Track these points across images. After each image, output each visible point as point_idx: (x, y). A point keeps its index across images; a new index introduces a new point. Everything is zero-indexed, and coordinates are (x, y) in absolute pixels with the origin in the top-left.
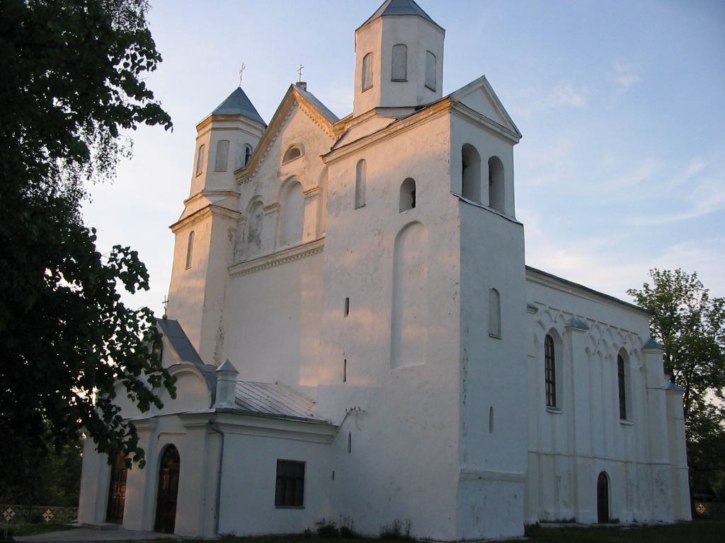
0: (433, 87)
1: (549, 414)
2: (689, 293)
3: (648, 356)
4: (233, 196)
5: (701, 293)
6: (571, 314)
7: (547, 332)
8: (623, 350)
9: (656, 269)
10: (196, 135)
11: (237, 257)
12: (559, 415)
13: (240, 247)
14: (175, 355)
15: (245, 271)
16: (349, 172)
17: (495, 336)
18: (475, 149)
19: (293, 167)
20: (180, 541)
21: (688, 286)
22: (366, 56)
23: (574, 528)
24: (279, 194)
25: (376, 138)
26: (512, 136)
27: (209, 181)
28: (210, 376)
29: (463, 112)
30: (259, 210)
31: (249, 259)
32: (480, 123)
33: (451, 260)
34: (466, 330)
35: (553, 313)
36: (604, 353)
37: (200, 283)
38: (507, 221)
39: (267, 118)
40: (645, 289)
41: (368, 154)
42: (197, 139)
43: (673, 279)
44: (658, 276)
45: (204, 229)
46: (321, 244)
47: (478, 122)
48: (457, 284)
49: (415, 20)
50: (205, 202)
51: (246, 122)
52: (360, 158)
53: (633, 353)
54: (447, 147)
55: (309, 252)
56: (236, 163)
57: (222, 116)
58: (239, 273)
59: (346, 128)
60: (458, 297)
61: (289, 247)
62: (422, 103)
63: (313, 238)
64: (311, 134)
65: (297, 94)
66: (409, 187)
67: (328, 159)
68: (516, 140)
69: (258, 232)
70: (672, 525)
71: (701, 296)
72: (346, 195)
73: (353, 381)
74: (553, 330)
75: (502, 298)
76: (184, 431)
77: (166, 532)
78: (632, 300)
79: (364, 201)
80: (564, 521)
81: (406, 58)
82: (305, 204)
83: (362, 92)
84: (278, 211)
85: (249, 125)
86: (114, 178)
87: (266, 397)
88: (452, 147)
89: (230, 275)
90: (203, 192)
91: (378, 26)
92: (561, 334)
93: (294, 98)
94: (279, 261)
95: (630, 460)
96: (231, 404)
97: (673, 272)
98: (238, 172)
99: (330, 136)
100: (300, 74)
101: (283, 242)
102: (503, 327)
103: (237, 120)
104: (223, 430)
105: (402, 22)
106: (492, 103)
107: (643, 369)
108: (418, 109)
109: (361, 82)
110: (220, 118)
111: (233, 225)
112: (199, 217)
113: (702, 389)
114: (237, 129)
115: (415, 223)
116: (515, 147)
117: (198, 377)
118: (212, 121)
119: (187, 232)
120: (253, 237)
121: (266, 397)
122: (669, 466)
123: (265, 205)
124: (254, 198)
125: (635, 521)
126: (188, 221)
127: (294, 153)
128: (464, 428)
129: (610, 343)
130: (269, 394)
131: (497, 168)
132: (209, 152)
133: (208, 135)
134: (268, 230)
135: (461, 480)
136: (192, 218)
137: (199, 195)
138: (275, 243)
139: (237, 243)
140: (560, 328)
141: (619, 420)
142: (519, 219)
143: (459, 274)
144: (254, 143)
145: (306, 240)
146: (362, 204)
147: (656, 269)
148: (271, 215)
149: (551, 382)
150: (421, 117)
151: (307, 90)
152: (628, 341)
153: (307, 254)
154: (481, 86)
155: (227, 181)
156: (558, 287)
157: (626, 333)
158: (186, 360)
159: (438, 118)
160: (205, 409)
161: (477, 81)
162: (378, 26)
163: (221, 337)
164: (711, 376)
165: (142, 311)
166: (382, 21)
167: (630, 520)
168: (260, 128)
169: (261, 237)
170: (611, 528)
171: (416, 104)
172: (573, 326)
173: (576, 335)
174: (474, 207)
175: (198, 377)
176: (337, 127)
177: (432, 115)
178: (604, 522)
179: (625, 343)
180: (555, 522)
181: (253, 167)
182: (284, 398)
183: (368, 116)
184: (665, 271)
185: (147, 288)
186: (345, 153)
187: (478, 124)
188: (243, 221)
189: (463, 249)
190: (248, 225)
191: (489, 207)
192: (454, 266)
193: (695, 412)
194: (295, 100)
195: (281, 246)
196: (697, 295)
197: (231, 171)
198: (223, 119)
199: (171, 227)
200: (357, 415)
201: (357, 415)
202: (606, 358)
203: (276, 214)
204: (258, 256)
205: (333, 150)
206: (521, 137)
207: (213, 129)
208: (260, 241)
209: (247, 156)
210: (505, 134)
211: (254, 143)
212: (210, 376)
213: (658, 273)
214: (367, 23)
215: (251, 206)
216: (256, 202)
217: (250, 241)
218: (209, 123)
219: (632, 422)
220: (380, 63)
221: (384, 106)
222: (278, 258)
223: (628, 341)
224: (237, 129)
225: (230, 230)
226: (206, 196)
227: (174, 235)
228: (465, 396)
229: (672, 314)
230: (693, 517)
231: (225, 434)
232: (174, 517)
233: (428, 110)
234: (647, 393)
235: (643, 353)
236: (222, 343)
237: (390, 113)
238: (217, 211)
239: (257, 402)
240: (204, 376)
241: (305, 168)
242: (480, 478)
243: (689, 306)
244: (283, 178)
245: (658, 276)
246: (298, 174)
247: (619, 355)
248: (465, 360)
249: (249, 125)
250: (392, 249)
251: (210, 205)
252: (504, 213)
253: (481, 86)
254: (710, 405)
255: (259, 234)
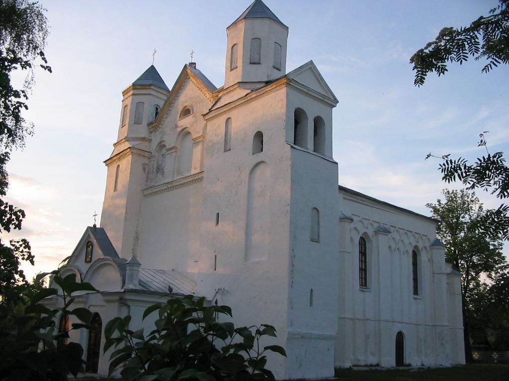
0: (279, 67)
1: (362, 292)
2: (470, 206)
3: (434, 251)
4: (147, 141)
5: (478, 206)
6: (378, 223)
7: (361, 235)
8: (416, 247)
9: (447, 189)
10: (122, 98)
11: (148, 183)
12: (368, 293)
13: (150, 176)
14: (100, 252)
15: (154, 193)
16: (221, 126)
17: (315, 240)
18: (302, 110)
19: (186, 122)
20: (98, 378)
21: (469, 201)
22: (234, 46)
23: (377, 371)
24: (177, 139)
25: (238, 103)
26: (331, 101)
27: (129, 131)
28: (122, 266)
29: (296, 86)
30: (164, 151)
31: (156, 185)
32: (308, 94)
33: (284, 190)
34: (294, 237)
35: (366, 222)
36: (402, 250)
37: (122, 202)
38: (326, 161)
39: (170, 84)
40: (438, 203)
41: (233, 114)
42: (123, 101)
43: (459, 196)
44: (448, 194)
45: (126, 163)
46: (202, 175)
47: (306, 92)
48: (288, 205)
49: (267, 21)
50: (127, 145)
51: (155, 89)
52: (228, 117)
53: (424, 249)
54: (284, 110)
55: (195, 180)
56: (148, 119)
57: (139, 85)
58: (150, 194)
59: (220, 96)
60: (288, 214)
61: (182, 177)
62: (271, 79)
63: (198, 171)
64: (198, 99)
65: (189, 71)
66: (259, 136)
67: (207, 117)
68: (334, 105)
69: (163, 165)
70: (447, 368)
71: (478, 208)
72: (218, 142)
73: (220, 270)
74: (365, 233)
75: (321, 214)
76: (105, 304)
77: (92, 372)
78: (429, 213)
79: (230, 147)
80: (371, 365)
81: (260, 48)
82: (193, 147)
83: (230, 71)
84: (176, 151)
85: (157, 91)
86: (24, 147)
87: (163, 280)
88: (287, 110)
89: (144, 195)
90: (126, 138)
91: (242, 26)
92: (371, 237)
93: (189, 73)
94: (176, 186)
95: (420, 323)
96: (136, 286)
97: (459, 191)
98: (149, 124)
99: (210, 101)
100: (192, 57)
101: (179, 173)
102: (322, 235)
103: (149, 89)
104: (129, 303)
105: (258, 22)
106: (318, 79)
107: (431, 260)
108: (268, 83)
109: (230, 64)
110: (138, 87)
111: (146, 161)
112: (122, 156)
113: (477, 273)
114: (149, 94)
115: (262, 162)
116: (334, 109)
117: (114, 267)
118: (133, 89)
119: (115, 165)
120: (159, 169)
121: (163, 280)
122: (448, 327)
123: (168, 147)
124: (160, 142)
125: (423, 365)
126: (115, 158)
127: (186, 112)
128: (291, 303)
129: (406, 242)
130: (165, 277)
131: (321, 126)
132: (130, 111)
133: (130, 99)
134: (169, 164)
135: (288, 339)
136: (118, 156)
137: (124, 140)
138: (174, 174)
139: (148, 173)
140: (370, 232)
141: (412, 295)
142: (335, 159)
143: (290, 198)
144: (161, 104)
145: (193, 172)
146: (228, 149)
147: (447, 189)
148: (171, 154)
149: (363, 270)
150: (267, 90)
151: (197, 68)
152: (420, 241)
153: (194, 182)
154: (310, 67)
155: (143, 130)
156: (368, 204)
157: (419, 235)
158: (108, 256)
159: (278, 90)
160: (118, 289)
161: (306, 64)
162: (242, 26)
163: (137, 239)
164: (483, 263)
165: (22, 241)
166: (244, 22)
167: (419, 364)
168: (165, 93)
169: (165, 170)
170: (404, 371)
171: (266, 79)
172: (379, 231)
173: (381, 237)
174: (303, 152)
175: (114, 267)
176: (215, 95)
177: (274, 88)
178: (399, 366)
179: (418, 242)
180: (364, 366)
181: (160, 121)
182: (176, 281)
183: (233, 88)
184: (453, 191)
185: (20, 228)
186: (217, 113)
187: (307, 94)
188: (153, 159)
189: (293, 181)
190: (156, 161)
191: (314, 151)
192: (287, 193)
193: (473, 289)
194: (188, 75)
195: (177, 176)
196: (475, 207)
197: (145, 123)
198: (140, 87)
199: (105, 162)
200: (223, 293)
201: (223, 293)
202: (404, 253)
203: (174, 153)
204: (162, 183)
205: (210, 111)
206: (338, 102)
207: (133, 94)
208: (164, 172)
209: (157, 113)
210: (326, 100)
211: (161, 104)
212: (122, 266)
213: (448, 192)
214: (235, 23)
215: (158, 148)
216: (161, 146)
217: (157, 172)
218: (130, 91)
219: (422, 297)
220: (242, 51)
221: (244, 81)
222: (175, 184)
223: (420, 241)
224: (149, 94)
225: (144, 164)
226: (127, 141)
227: (107, 167)
228: (293, 281)
229: (458, 221)
230: (466, 362)
231: (131, 307)
232: (97, 362)
233: (272, 85)
234: (433, 277)
235: (431, 249)
236: (138, 242)
237: (248, 86)
238: (135, 151)
239: (156, 284)
240: (118, 267)
241: (194, 122)
242: (302, 337)
243: (469, 215)
244: (179, 129)
245: (448, 194)
246: (189, 126)
247: (413, 250)
248: (293, 257)
249: (157, 91)
250: (247, 179)
251: (130, 148)
252: (324, 155)
253: (310, 67)
254: (484, 284)
255: (164, 168)
